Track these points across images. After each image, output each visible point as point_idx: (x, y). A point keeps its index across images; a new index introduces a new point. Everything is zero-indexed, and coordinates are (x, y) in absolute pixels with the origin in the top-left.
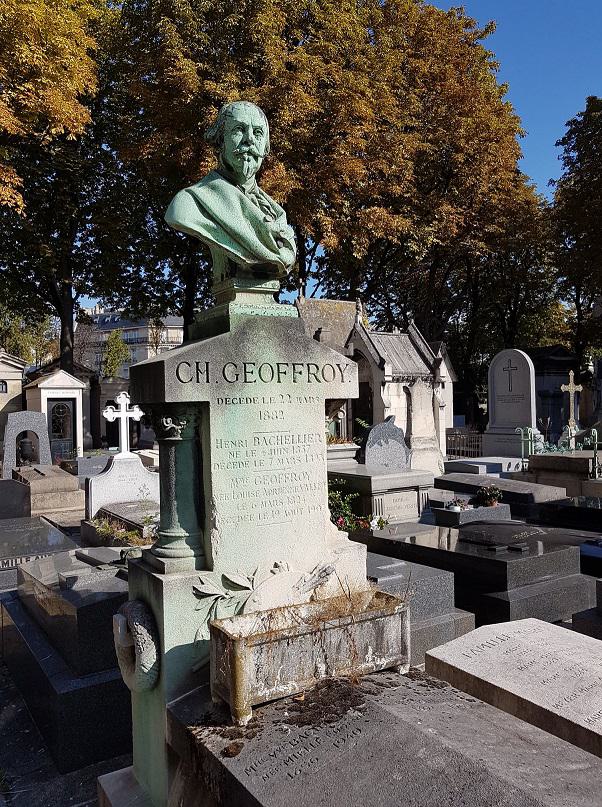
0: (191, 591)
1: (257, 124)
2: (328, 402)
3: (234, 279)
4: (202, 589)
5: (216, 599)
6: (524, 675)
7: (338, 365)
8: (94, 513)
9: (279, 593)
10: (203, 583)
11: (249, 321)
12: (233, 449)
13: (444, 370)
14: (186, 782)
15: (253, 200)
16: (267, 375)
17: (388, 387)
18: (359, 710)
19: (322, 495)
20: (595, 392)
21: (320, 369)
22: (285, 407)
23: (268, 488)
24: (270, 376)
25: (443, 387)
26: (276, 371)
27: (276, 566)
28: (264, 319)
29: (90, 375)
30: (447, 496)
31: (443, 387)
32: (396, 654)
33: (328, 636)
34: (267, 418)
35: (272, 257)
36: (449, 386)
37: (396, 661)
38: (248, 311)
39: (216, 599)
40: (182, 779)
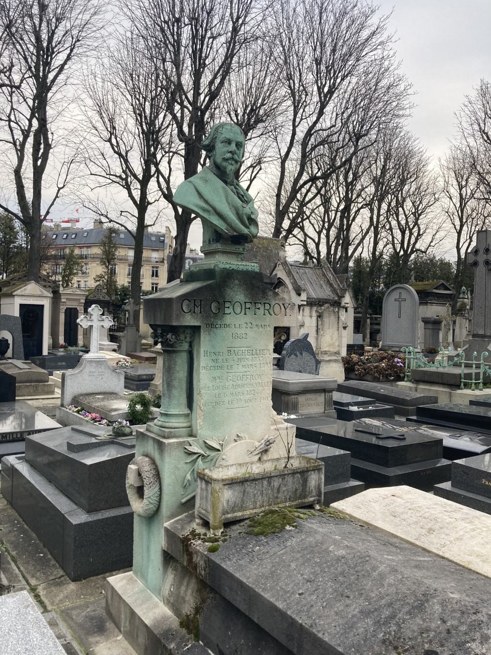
0: (183, 451)
1: (239, 140)
2: (276, 328)
3: (218, 244)
4: (191, 449)
5: (199, 456)
6: (397, 520)
7: (283, 304)
8: (68, 398)
9: (235, 460)
10: (191, 445)
11: (228, 274)
12: (214, 357)
13: (347, 299)
14: (175, 575)
15: (232, 190)
16: (238, 310)
17: (303, 310)
18: (293, 526)
19: (269, 391)
20: (468, 321)
21: (272, 306)
22: (248, 331)
23: (235, 384)
24: (240, 310)
25: (346, 311)
26: (243, 307)
27: (238, 436)
28: (238, 272)
29: (52, 285)
30: (346, 398)
31: (346, 311)
32: (314, 496)
33: (272, 481)
34: (236, 337)
35: (246, 231)
36: (351, 311)
37: (314, 501)
38: (228, 266)
39: (199, 456)
40: (172, 573)
